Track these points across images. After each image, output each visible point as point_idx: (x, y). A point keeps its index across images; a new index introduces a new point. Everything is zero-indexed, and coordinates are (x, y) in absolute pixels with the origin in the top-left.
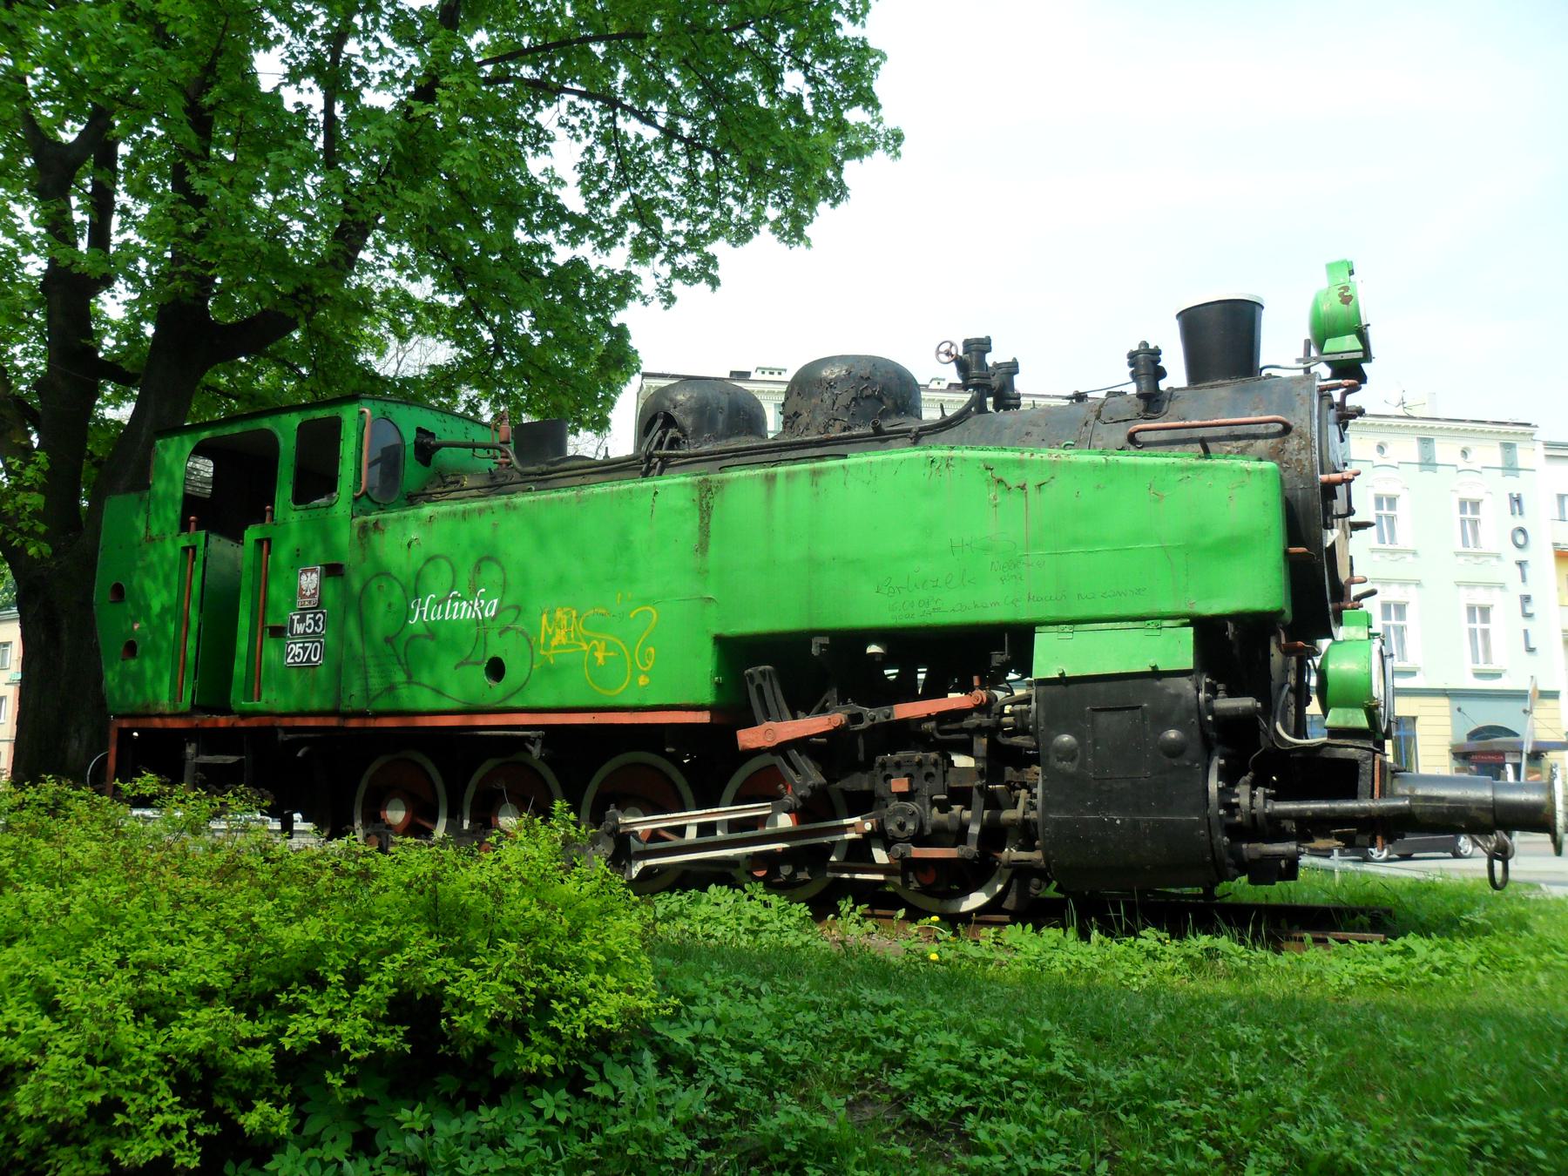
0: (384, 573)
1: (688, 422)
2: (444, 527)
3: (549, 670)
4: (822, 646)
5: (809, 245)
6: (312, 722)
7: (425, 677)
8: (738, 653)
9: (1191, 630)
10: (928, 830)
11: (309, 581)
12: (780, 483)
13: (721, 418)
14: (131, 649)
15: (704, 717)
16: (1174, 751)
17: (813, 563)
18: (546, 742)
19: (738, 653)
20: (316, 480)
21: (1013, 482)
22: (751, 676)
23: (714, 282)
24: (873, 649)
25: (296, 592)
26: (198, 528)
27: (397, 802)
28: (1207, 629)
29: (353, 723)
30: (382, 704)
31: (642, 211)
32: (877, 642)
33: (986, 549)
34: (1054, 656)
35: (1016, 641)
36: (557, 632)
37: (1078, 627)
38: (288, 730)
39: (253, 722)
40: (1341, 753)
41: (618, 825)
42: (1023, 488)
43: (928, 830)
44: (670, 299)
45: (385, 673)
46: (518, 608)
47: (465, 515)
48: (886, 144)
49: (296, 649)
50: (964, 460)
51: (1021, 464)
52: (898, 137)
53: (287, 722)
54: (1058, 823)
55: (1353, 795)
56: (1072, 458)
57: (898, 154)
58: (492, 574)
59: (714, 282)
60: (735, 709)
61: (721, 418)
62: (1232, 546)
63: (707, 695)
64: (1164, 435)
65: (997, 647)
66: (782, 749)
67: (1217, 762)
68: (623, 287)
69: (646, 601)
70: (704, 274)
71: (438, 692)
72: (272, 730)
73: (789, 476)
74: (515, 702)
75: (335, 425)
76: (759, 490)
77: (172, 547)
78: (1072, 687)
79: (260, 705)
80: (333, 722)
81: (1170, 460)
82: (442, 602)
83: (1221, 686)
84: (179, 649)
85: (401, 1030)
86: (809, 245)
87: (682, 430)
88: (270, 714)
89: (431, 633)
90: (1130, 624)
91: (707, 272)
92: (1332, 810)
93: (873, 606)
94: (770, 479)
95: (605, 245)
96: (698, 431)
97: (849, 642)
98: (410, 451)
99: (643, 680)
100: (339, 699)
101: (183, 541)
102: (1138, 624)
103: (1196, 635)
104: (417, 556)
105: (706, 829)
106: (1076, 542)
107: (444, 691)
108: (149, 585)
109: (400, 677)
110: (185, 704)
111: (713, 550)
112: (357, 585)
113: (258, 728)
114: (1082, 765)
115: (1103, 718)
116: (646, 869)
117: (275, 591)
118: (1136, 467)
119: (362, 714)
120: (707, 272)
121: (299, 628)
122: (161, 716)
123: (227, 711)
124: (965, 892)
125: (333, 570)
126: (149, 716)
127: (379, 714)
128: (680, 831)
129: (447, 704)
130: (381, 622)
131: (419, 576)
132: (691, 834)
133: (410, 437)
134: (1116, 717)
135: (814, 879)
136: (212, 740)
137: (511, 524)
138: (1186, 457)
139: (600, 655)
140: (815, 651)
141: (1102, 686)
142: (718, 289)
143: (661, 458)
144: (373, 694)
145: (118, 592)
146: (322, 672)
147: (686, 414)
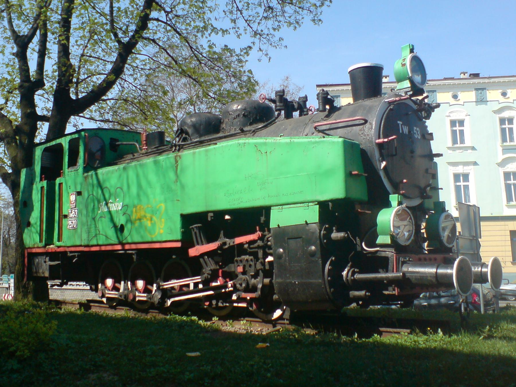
4: (211, 217)
8: (188, 220)
11: (73, 198)
15: (179, 245)
16: (313, 254)
19: (188, 220)
21: (263, 152)
22: (192, 228)
24: (227, 217)
26: (45, 180)
28: (323, 205)
32: (229, 215)
34: (278, 219)
35: (266, 210)
37: (284, 207)
38: (71, 252)
40: (383, 254)
50: (249, 143)
51: (265, 144)
53: (73, 249)
55: (387, 271)
56: (333, 140)
60: (187, 241)
62: (329, 173)
63: (179, 237)
64: (327, 127)
65: (255, 218)
66: (202, 255)
72: (65, 252)
73: (199, 152)
81: (310, 140)
90: (299, 205)
92: (376, 278)
93: (224, 201)
94: (194, 153)
97: (219, 214)
98: (107, 147)
102: (302, 205)
103: (319, 208)
105: (196, 285)
115: (292, 242)
116: (172, 302)
127: (92, 246)
128: (188, 286)
132: (192, 287)
138: (317, 138)
140: (209, 219)
143: (179, 145)
144: (95, 238)
147: (189, 128)
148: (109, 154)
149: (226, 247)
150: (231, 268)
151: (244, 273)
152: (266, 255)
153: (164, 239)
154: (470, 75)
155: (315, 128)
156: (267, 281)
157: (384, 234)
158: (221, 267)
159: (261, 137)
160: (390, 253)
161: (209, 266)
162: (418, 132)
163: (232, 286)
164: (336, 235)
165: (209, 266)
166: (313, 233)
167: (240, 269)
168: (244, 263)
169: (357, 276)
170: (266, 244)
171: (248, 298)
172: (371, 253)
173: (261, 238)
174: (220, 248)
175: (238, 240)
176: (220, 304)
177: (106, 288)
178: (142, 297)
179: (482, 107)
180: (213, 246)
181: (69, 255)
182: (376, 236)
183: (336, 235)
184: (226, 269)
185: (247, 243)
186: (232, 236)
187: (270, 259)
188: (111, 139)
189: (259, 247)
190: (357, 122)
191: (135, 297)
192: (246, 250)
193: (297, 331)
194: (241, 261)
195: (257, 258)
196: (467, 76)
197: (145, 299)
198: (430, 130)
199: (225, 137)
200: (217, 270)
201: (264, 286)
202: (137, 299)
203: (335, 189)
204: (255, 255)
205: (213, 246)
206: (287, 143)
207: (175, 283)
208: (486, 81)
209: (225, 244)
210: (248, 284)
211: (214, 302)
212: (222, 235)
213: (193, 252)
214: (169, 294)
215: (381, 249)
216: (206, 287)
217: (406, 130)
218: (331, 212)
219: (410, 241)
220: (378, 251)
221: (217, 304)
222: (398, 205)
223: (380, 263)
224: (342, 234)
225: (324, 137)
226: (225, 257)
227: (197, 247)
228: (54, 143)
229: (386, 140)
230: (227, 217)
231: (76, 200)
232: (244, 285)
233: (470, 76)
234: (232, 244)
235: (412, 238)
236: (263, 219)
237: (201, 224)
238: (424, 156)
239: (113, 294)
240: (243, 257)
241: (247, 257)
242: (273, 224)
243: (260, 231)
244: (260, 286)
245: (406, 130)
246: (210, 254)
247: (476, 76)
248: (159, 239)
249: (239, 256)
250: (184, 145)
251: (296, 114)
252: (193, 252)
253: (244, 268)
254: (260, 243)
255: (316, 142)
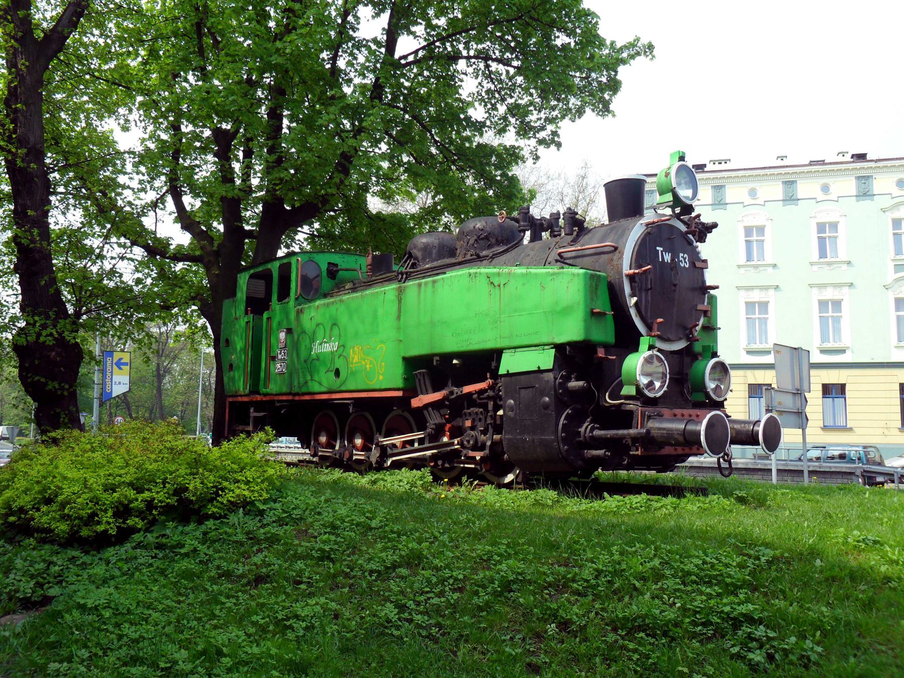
0: (304, 332)
1: (419, 254)
2: (321, 310)
3: (353, 373)
5: (614, 116)
6: (284, 398)
7: (316, 378)
9: (554, 350)
10: (479, 444)
11: (282, 335)
12: (423, 285)
13: (434, 251)
14: (231, 366)
15: (400, 394)
16: (546, 407)
17: (432, 323)
18: (355, 405)
19: (412, 363)
20: (284, 294)
21: (496, 284)
23: (559, 145)
24: (455, 361)
25: (278, 340)
27: (358, 435)
28: (559, 348)
29: (297, 398)
30: (304, 390)
31: (515, 110)
33: (487, 315)
34: (509, 364)
35: (496, 354)
36: (355, 357)
38: (279, 401)
39: (268, 398)
41: (379, 442)
42: (499, 286)
43: (479, 444)
44: (537, 158)
45: (305, 377)
46: (343, 346)
47: (328, 305)
48: (645, 52)
49: (278, 366)
52: (651, 47)
54: (509, 440)
57: (653, 56)
58: (336, 331)
59: (559, 145)
60: (411, 391)
61: (434, 251)
62: (567, 311)
63: (400, 383)
64: (573, 254)
65: (484, 362)
66: (426, 406)
67: (569, 411)
68: (512, 155)
69: (382, 342)
70: (553, 141)
71: (320, 384)
72: (273, 402)
73: (426, 283)
74: (343, 388)
75: (289, 264)
76: (416, 289)
77: (243, 322)
78: (514, 378)
79: (268, 391)
80: (290, 398)
82: (321, 344)
83: (59, 392)
84: (245, 365)
85: (176, 498)
86: (614, 116)
87: (416, 258)
88: (272, 395)
89: (318, 356)
91: (553, 141)
93: (451, 343)
94: (420, 285)
95: (501, 131)
96: (424, 259)
97: (446, 357)
98: (324, 274)
99: (381, 377)
100: (291, 388)
101: (246, 320)
104: (314, 323)
106: (516, 311)
107: (321, 384)
108: (236, 339)
109: (309, 378)
110: (247, 391)
111: (402, 318)
112: (296, 337)
113: (215, 399)
114: (516, 414)
116: (393, 461)
117: (273, 340)
118: (536, 274)
119: (298, 394)
120: (553, 141)
121: (280, 357)
122: (241, 396)
123: (259, 393)
124: (506, 475)
125: (289, 331)
126: (237, 396)
129: (323, 389)
130: (303, 354)
131: (314, 332)
133: (324, 267)
134: (527, 391)
135: (447, 468)
136: (259, 406)
137: (342, 308)
139: (368, 366)
141: (523, 377)
142: (561, 149)
143: (406, 273)
145: (227, 341)
146: (286, 375)
148: (326, 283)
149: (453, 397)
150: (458, 422)
151: (473, 428)
152: (497, 408)
153: (383, 387)
154: (853, 156)
155: (559, 254)
156: (497, 437)
157: (630, 384)
158: (448, 421)
159: (505, 264)
160: (632, 406)
161: (434, 419)
162: (685, 259)
163: (458, 444)
164: (574, 384)
165: (434, 419)
166: (548, 381)
167: (468, 423)
168: (473, 416)
169: (597, 433)
170: (498, 394)
171: (478, 458)
172: (614, 405)
173: (491, 387)
174: (445, 398)
175: (467, 389)
176: (447, 465)
177: (319, 444)
178: (359, 455)
179: (866, 203)
180: (437, 396)
181: (278, 404)
182: (621, 385)
183: (574, 384)
184: (455, 423)
185: (476, 392)
186: (460, 385)
187: (501, 412)
188: (329, 263)
189: (489, 398)
190: (606, 249)
191: (352, 455)
192: (475, 401)
193: (124, 523)
194: (470, 414)
195: (487, 411)
196: (848, 158)
197: (363, 458)
198: (703, 256)
199: (460, 263)
200: (443, 425)
201: (494, 444)
202: (355, 457)
203: (572, 330)
204: (485, 406)
205: (437, 396)
206: (523, 275)
207: (397, 440)
208: (873, 164)
209: (452, 393)
210: (476, 441)
211: (440, 462)
212: (450, 384)
213: (416, 403)
214: (389, 451)
215: (627, 402)
216: (421, 447)
217: (668, 258)
218: (571, 356)
219: (662, 392)
220: (622, 404)
221: (443, 465)
222: (649, 349)
223: (624, 418)
224: (581, 383)
225: (562, 268)
226: (456, 407)
227: (421, 396)
228: (260, 269)
229: (637, 271)
230: (455, 361)
231: (286, 339)
232: (471, 442)
233: (852, 157)
234: (459, 393)
235: (665, 388)
236: (494, 364)
237: (428, 369)
238: (694, 289)
239: (328, 452)
240: (472, 409)
241: (476, 410)
242: (502, 371)
243: (491, 378)
244: (489, 443)
245: (668, 258)
246: (436, 405)
247: (861, 157)
248: (377, 387)
249: (468, 409)
250: (411, 272)
251: (545, 235)
252: (416, 403)
253: (473, 422)
254: (490, 393)
255: (553, 274)
